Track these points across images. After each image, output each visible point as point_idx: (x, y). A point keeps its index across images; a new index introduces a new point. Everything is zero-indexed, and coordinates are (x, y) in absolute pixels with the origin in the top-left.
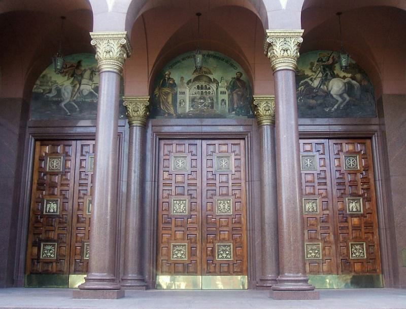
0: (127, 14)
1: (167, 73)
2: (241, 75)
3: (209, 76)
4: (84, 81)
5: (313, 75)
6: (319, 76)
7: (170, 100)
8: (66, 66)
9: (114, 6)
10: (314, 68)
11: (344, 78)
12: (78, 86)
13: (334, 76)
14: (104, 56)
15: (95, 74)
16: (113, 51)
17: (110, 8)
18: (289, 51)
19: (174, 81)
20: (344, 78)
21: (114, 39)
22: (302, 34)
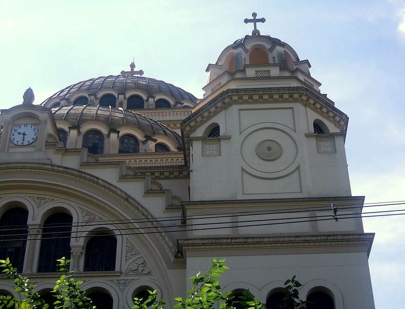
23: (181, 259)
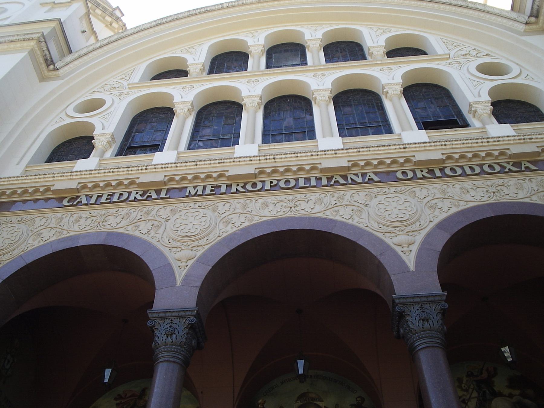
0: (201, 288)
1: (260, 401)
2: (363, 400)
3: (318, 403)
5: (464, 395)
6: (473, 396)
8: (126, 395)
9: (184, 280)
10: (463, 385)
11: (511, 396)
13: (496, 394)
14: (164, 339)
16: (177, 333)
17: (179, 282)
18: (430, 322)
20: (511, 396)
22: (444, 298)
23: (534, 27)
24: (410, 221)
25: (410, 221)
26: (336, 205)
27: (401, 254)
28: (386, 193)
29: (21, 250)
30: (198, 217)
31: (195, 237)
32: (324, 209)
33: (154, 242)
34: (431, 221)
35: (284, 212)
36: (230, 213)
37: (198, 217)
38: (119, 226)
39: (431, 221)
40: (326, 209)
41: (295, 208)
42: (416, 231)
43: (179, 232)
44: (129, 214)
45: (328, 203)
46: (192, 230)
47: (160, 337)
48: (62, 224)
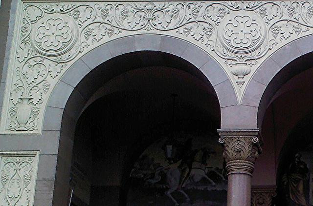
1: (297, 155)
4: (195, 165)
7: (301, 188)
12: (188, 170)
15: (209, 156)
17: (240, 98)
19: (305, 165)
21: (245, 137)
24: (252, 48)
25: (252, 48)
26: (190, 21)
27: (235, 85)
28: (53, 12)
29: (78, 50)
30: (248, 24)
31: (246, 51)
32: (178, 25)
33: (208, 50)
34: (271, 49)
35: (142, 25)
36: (90, 21)
37: (248, 24)
38: (170, 27)
39: (271, 49)
40: (181, 25)
41: (153, 22)
42: (254, 59)
43: (42, 44)
44: (176, 12)
45: (183, 18)
46: (245, 41)
47: (232, 147)
48: (108, 18)
